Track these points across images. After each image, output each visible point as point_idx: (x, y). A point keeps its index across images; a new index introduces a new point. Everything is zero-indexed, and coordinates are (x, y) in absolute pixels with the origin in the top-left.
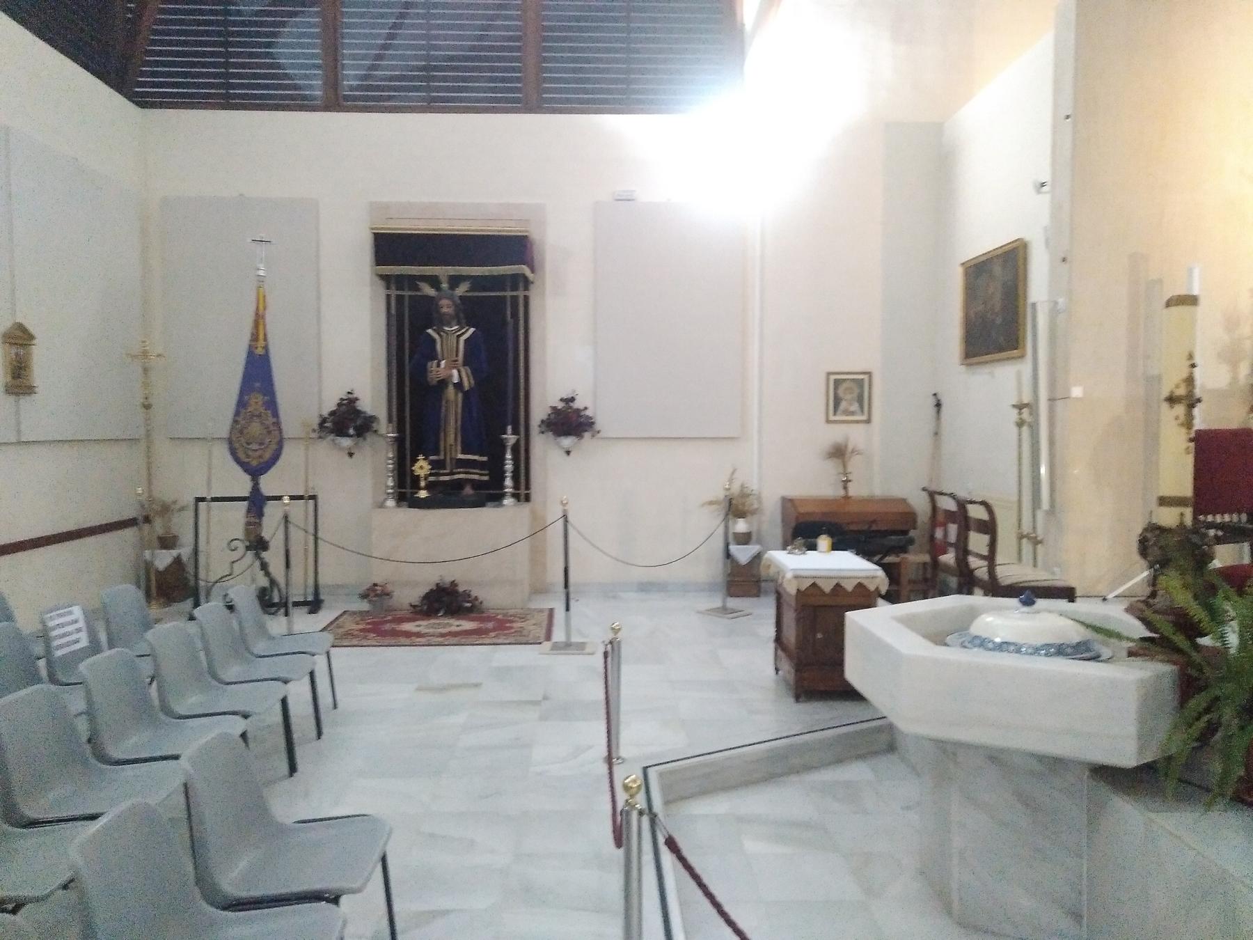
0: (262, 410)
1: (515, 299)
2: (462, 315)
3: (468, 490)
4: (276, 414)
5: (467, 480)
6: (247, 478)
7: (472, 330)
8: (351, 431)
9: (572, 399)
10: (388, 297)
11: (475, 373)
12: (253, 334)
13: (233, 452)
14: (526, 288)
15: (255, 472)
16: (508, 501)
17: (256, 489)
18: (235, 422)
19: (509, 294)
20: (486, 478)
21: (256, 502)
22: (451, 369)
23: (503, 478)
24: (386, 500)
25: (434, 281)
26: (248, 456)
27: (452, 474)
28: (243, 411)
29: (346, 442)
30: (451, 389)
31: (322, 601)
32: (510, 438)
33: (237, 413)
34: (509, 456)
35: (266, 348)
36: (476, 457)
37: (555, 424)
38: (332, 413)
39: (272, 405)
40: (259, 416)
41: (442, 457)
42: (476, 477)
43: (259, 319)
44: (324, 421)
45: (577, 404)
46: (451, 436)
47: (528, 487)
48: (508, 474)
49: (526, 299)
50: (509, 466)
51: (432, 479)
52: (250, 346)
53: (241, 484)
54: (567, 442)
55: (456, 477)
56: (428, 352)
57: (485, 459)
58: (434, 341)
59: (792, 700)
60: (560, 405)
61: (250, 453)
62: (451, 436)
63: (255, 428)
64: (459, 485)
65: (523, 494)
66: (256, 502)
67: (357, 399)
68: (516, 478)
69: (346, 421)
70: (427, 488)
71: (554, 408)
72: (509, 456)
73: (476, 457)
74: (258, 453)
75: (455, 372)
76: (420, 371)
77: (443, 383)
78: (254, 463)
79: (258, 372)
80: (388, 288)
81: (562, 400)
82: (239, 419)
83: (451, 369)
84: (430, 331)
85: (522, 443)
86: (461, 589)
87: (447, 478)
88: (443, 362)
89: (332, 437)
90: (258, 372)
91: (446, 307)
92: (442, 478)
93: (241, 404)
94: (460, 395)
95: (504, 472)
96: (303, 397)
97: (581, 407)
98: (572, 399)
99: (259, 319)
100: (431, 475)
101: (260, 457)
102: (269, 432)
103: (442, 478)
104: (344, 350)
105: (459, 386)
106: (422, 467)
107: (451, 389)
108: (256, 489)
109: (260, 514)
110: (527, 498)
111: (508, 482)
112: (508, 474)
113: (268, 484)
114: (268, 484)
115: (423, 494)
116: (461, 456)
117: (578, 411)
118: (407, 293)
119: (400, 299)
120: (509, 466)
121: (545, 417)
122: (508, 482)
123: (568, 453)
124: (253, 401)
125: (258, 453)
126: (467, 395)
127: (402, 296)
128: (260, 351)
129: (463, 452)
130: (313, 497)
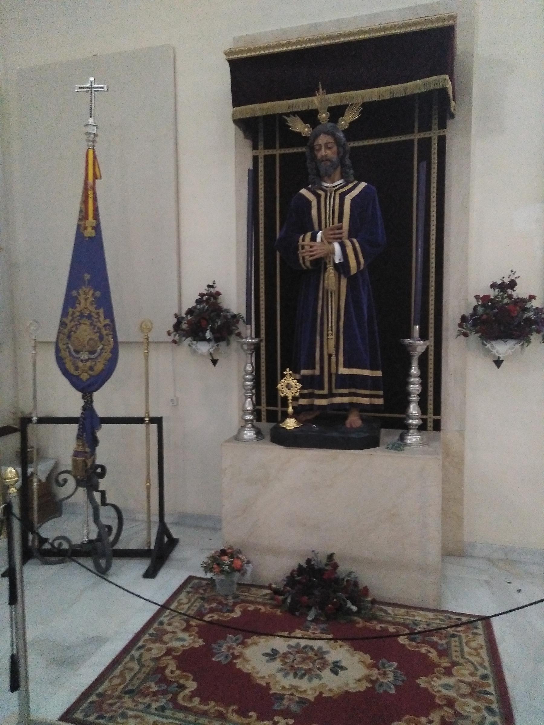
0: (92, 308)
1: (425, 144)
2: (348, 162)
3: (354, 420)
4: (109, 314)
5: (352, 405)
6: (80, 394)
7: (363, 185)
8: (208, 335)
9: (512, 284)
10: (255, 159)
11: (368, 247)
12: (81, 211)
13: (60, 361)
14: (443, 125)
15: (87, 388)
16: (413, 438)
17: (88, 408)
18: (63, 324)
19: (416, 136)
20: (380, 401)
21: (89, 425)
22: (331, 245)
23: (408, 403)
24: (243, 427)
25: (310, 117)
26: (77, 368)
27: (331, 395)
28: (71, 310)
29: (204, 348)
30: (331, 272)
31: (173, 543)
32: (419, 345)
33: (65, 313)
34: (415, 370)
35: (97, 228)
36: (366, 372)
37: (484, 322)
38: (190, 312)
39: (104, 302)
40: (89, 317)
41: (317, 372)
42: (365, 401)
43: (89, 192)
44: (179, 320)
45: (520, 292)
46: (330, 340)
47: (437, 410)
48: (414, 398)
49: (442, 140)
50: (415, 387)
51: (303, 402)
52: (79, 226)
53: (71, 403)
54: (501, 348)
55: (337, 400)
56: (300, 221)
57: (379, 373)
58: (308, 203)
59: (252, 149)
60: (492, 293)
61: (80, 364)
62: (330, 340)
63: (85, 333)
64: (338, 414)
65: (432, 424)
66: (89, 425)
67: (218, 294)
68: (423, 405)
69: (204, 322)
70: (296, 414)
71: (486, 298)
72: (415, 370)
73: (366, 372)
74: (88, 364)
75: (337, 246)
76: (291, 249)
77: (320, 264)
78: (85, 377)
79: (89, 258)
80: (255, 147)
81: (494, 286)
82: (67, 321)
83: (331, 245)
84: (303, 191)
85: (431, 353)
86: (343, 568)
87: (324, 402)
88: (319, 234)
89: (189, 340)
90: (89, 258)
91: (326, 148)
92: (318, 402)
93: (70, 301)
94: (344, 282)
95: (409, 394)
96: (148, 290)
97: (526, 296)
98: (512, 284)
99: (89, 192)
100: (302, 396)
101: (91, 368)
102: (101, 338)
103: (318, 402)
104: (197, 227)
105: (342, 268)
106: (289, 386)
107: (331, 272)
108: (88, 408)
109: (94, 442)
110: (437, 426)
111: (414, 409)
112: (414, 398)
113: (105, 402)
114: (105, 402)
115: (291, 424)
116: (343, 371)
117: (523, 301)
118: (277, 152)
119: (269, 161)
120: (415, 387)
121: (468, 312)
122: (414, 409)
123: (498, 363)
124: (82, 298)
125: (88, 364)
126: (353, 281)
127: (273, 157)
128: (89, 232)
129: (347, 365)
130: (158, 421)
